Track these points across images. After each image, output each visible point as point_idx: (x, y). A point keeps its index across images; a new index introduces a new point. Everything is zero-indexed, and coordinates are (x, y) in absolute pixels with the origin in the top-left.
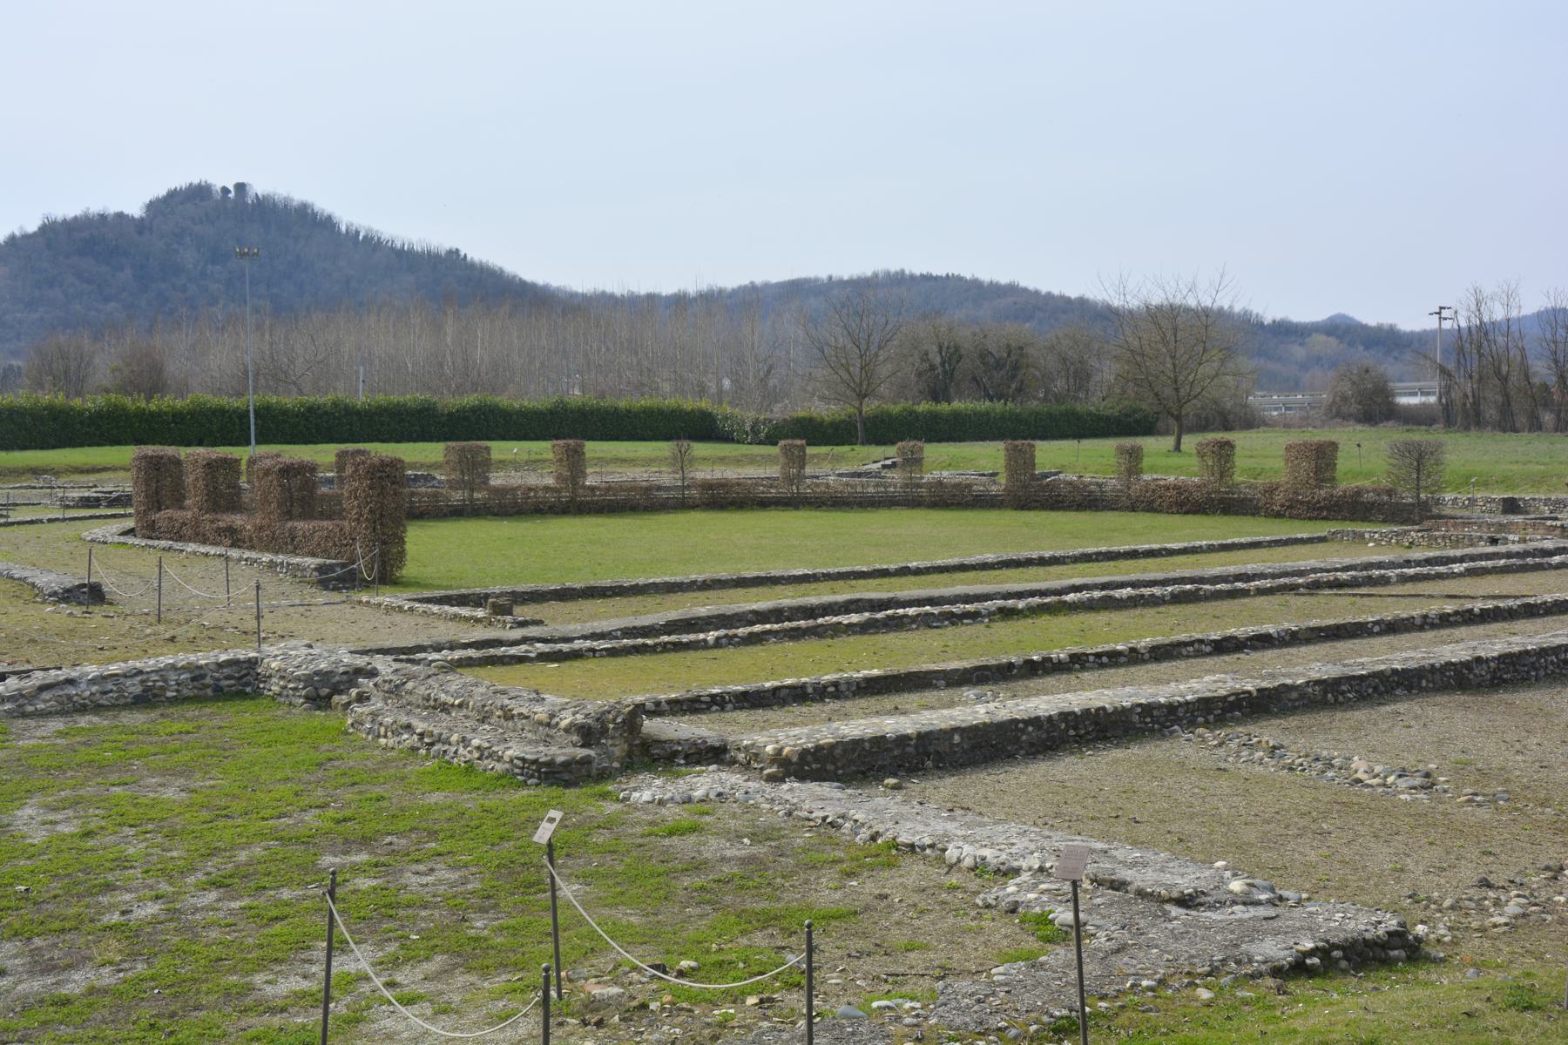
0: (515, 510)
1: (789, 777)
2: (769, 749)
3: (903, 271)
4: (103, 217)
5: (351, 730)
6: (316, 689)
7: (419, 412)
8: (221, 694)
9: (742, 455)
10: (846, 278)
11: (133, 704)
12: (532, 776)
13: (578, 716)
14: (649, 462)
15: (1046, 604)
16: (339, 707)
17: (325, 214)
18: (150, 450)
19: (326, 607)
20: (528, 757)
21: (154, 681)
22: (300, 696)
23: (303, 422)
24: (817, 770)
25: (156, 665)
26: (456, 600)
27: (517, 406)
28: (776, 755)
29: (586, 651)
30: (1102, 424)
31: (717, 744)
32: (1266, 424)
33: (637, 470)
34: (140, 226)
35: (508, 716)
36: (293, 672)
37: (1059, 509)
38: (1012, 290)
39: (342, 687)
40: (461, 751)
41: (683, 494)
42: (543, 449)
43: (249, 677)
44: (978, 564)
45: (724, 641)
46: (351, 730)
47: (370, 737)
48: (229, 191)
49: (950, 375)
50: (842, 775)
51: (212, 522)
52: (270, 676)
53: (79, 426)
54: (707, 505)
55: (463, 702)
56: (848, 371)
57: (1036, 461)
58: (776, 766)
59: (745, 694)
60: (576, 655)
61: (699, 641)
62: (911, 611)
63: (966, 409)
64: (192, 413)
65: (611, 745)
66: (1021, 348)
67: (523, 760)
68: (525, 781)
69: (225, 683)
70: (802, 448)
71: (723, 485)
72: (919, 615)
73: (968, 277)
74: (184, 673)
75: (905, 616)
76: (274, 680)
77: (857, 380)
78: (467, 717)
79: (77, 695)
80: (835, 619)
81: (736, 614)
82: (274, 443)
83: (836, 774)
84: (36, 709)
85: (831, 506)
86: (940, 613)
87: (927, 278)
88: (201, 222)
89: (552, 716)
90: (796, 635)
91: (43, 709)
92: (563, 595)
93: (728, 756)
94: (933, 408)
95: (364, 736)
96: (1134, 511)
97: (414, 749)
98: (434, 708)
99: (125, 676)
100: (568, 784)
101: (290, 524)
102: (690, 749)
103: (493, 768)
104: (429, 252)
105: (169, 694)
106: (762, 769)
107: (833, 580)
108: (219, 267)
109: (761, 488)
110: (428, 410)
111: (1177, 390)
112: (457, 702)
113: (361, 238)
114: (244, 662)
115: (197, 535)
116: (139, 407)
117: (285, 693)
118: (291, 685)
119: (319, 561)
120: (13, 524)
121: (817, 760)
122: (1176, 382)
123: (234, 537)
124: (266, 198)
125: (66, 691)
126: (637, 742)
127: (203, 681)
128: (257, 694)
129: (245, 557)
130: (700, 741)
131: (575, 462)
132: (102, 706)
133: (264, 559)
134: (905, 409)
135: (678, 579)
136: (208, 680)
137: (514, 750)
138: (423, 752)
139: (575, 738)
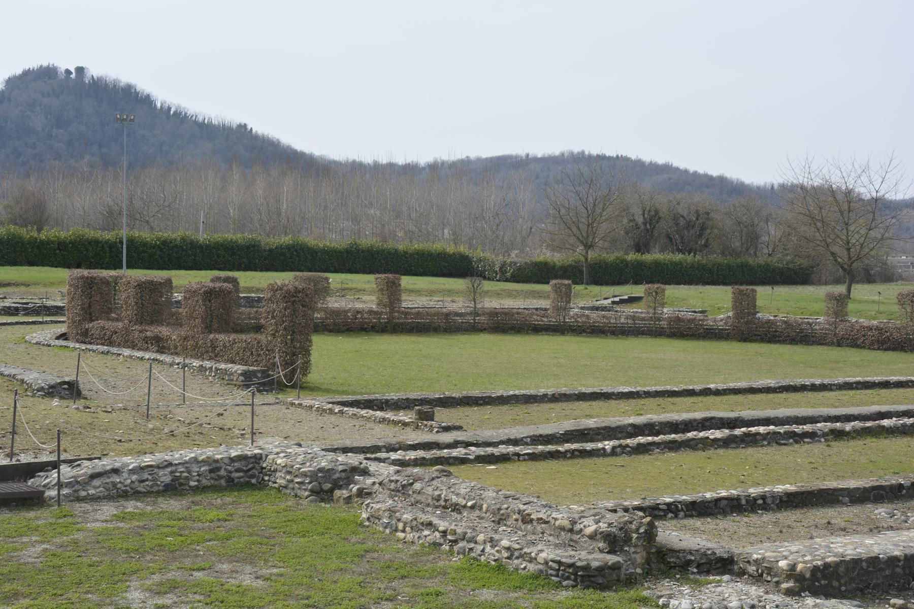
0: (345, 328)
1: (804, 592)
2: (783, 564)
3: (583, 152)
5: (367, 523)
6: (320, 483)
7: (248, 247)
8: (232, 485)
10: (539, 156)
11: (163, 491)
12: (568, 578)
13: (601, 524)
14: (431, 293)
15: (868, 428)
16: (341, 500)
17: (145, 93)
18: (85, 272)
19: (264, 407)
20: (564, 560)
21: (181, 472)
22: (305, 490)
23: (158, 252)
24: (826, 586)
25: (181, 459)
27: (321, 246)
28: (791, 570)
29: (513, 455)
30: (769, 275)
31: (726, 556)
32: (903, 279)
33: (424, 299)
35: (526, 519)
36: (300, 469)
37: (775, 342)
38: (667, 169)
39: (341, 483)
40: (488, 549)
41: (474, 320)
43: (254, 471)
44: (763, 388)
45: (618, 450)
46: (367, 523)
47: (388, 531)
48: (71, 73)
49: (650, 232)
50: (845, 591)
51: (140, 332)
52: (275, 471)
54: (493, 329)
56: (579, 229)
57: (757, 304)
58: (792, 581)
60: (504, 458)
61: (599, 450)
62: (762, 429)
63: (664, 259)
64: (73, 243)
65: (633, 553)
66: (708, 214)
67: (559, 563)
69: (235, 475)
70: (569, 287)
71: (508, 313)
72: (768, 433)
73: (633, 157)
74: (204, 466)
75: (758, 434)
76: (278, 474)
77: (585, 235)
78: (481, 518)
79: (120, 482)
80: (702, 434)
81: (618, 427)
82: (136, 268)
83: (840, 590)
84: (88, 494)
85: (590, 333)
86: (785, 433)
87: (601, 158)
88: (49, 95)
89: (574, 523)
90: (673, 446)
91: (94, 495)
92: (446, 403)
93: (736, 567)
94: (638, 258)
95: (381, 529)
96: (839, 346)
97: (436, 545)
98: (445, 507)
99: (158, 467)
100: (603, 588)
101: (211, 336)
102: (701, 558)
103: (525, 568)
105: (192, 483)
106: (777, 583)
107: (652, 397)
108: (61, 131)
109: (535, 317)
110: (254, 246)
111: (849, 250)
112: (469, 504)
113: (172, 112)
114: (251, 457)
115: (127, 342)
116: (31, 236)
117: (291, 486)
118: (299, 480)
119: (245, 368)
121: (825, 577)
122: (848, 243)
123: (160, 344)
124: (100, 79)
125: (111, 480)
126: (653, 550)
127: (219, 473)
128: (262, 486)
129: (177, 362)
130: (709, 552)
131: (392, 292)
132: (139, 492)
133: (194, 364)
134: (617, 258)
135: (532, 392)
136: (222, 473)
137: (548, 554)
138: (446, 547)
139: (601, 545)
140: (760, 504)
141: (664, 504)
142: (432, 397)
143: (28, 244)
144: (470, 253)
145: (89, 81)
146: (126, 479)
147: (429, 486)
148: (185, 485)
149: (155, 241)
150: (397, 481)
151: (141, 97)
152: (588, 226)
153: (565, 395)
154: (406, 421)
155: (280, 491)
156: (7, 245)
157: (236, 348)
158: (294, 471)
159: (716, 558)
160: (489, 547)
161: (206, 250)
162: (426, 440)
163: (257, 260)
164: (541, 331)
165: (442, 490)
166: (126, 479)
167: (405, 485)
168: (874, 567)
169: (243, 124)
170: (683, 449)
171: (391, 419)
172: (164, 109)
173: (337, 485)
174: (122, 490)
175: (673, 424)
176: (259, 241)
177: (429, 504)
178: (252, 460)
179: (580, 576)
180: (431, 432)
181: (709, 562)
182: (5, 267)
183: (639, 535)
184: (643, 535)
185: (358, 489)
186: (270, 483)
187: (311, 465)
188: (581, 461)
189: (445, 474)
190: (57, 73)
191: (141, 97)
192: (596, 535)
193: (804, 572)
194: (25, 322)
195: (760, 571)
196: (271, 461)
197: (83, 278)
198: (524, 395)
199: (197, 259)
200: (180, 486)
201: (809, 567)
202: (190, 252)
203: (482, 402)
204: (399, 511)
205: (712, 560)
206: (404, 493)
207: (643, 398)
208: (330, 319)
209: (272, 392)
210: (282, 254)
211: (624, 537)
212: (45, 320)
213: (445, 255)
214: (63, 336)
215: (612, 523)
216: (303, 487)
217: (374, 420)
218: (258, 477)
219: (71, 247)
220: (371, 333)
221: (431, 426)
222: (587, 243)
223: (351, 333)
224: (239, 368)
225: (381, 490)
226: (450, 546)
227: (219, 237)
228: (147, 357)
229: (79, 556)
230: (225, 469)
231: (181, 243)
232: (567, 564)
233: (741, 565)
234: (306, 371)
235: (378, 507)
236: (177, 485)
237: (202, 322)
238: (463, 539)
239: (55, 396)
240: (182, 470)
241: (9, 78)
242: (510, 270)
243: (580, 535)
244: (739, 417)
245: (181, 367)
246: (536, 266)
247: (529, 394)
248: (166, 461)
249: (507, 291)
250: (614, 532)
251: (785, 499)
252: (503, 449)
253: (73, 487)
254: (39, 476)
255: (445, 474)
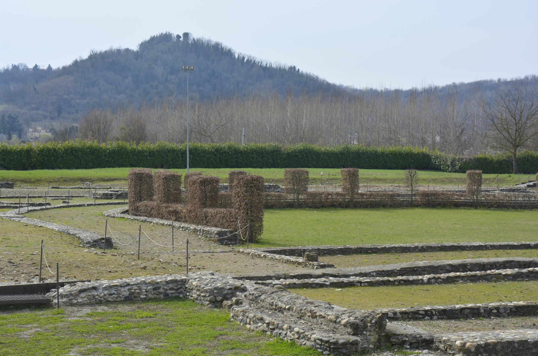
2: (458, 343)
4: (119, 51)
5: (232, 320)
6: (215, 297)
7: (273, 152)
8: (167, 298)
9: (445, 178)
10: (508, 80)
11: (124, 301)
12: (326, 350)
13: (351, 318)
14: (393, 181)
16: (227, 307)
17: (228, 49)
18: (137, 170)
20: (324, 339)
21: (135, 290)
22: (207, 300)
23: (213, 157)
26: (288, 252)
27: (323, 149)
28: (462, 346)
31: (428, 338)
34: (136, 55)
35: (314, 316)
39: (228, 297)
40: (289, 333)
41: (412, 199)
42: (336, 173)
43: (181, 289)
45: (433, 280)
46: (232, 320)
47: (242, 324)
52: (192, 289)
53: (104, 157)
54: (425, 205)
55: (290, 307)
56: (508, 132)
59: (444, 311)
60: (351, 285)
61: (418, 280)
64: (158, 151)
65: (369, 335)
67: (321, 340)
68: (322, 352)
69: (169, 292)
70: (480, 175)
71: (435, 194)
74: (149, 286)
76: (194, 291)
77: (513, 137)
78: (292, 315)
79: (97, 295)
81: (440, 266)
82: (199, 167)
84: (78, 301)
85: (496, 207)
89: (337, 317)
90: (474, 279)
91: (81, 302)
92: (345, 252)
93: (434, 345)
97: (264, 331)
98: (275, 310)
99: (121, 286)
101: (205, 210)
102: (413, 340)
103: (305, 344)
104: (280, 68)
105: (142, 297)
107: (496, 249)
109: (456, 197)
110: (276, 151)
112: (287, 307)
113: (245, 61)
114: (179, 281)
118: (203, 294)
119: (219, 229)
120: (71, 206)
123: (177, 216)
124: (198, 40)
125: (92, 293)
126: (383, 334)
127: (159, 291)
128: (185, 298)
130: (418, 336)
131: (353, 180)
133: (191, 228)
135: (408, 245)
136: (161, 290)
139: (349, 330)
140: (495, 313)
141: (423, 311)
142: (336, 248)
143: (130, 153)
144: (431, 153)
145: (192, 42)
146: (101, 293)
147: (269, 297)
148: (138, 297)
149: (211, 149)
150: (253, 294)
151: (225, 51)
152: (516, 131)
153: (431, 247)
154: (300, 262)
155: (194, 301)
156: (118, 154)
157: (218, 217)
158: (200, 289)
159: (422, 340)
160: (289, 332)
161: (245, 154)
162: (303, 273)
163: (279, 161)
164: (460, 206)
165: (275, 299)
166: (101, 293)
167: (257, 296)
168: (523, 347)
169: (293, 67)
170: (480, 281)
171: (292, 261)
172: (240, 59)
173: (225, 298)
174: (98, 300)
175: (481, 265)
176: (280, 148)
177: (267, 308)
178: (180, 283)
179: (332, 348)
180: (313, 268)
181: (418, 342)
182: (115, 168)
183: (372, 324)
184: (374, 324)
185: (236, 300)
186: (190, 297)
187: (211, 285)
188: (403, 287)
189: (281, 290)
190: (171, 38)
191: (225, 51)
192: (347, 324)
193: (470, 348)
194: (113, 203)
195: (446, 347)
196: (190, 284)
197: (135, 174)
198: (401, 247)
199: (239, 160)
200: (135, 298)
201: (474, 345)
202: (234, 156)
203: (371, 251)
204: (248, 312)
205: (419, 341)
206: (256, 301)
207: (490, 250)
208: (310, 199)
209: (236, 245)
210: (296, 156)
211: (363, 325)
212: (125, 202)
213: (411, 154)
214: (126, 212)
215: (357, 317)
216: (206, 299)
217: (282, 261)
218: (184, 293)
219: (157, 155)
220: (338, 208)
221: (313, 265)
222: (515, 144)
223: (325, 208)
224: (215, 230)
225: (245, 300)
226: (271, 332)
227: (253, 145)
228: (166, 223)
229: (54, 335)
230: (163, 288)
231: (228, 150)
232: (325, 341)
233: (437, 344)
234: (260, 231)
235: (237, 310)
236: (133, 298)
237: (199, 201)
238: (277, 328)
239: (97, 247)
240: (136, 288)
241: (142, 43)
242: (458, 164)
243: (339, 325)
244: (532, 261)
245: (184, 230)
246: (477, 161)
247: (405, 246)
248: (126, 283)
249: (450, 179)
250: (357, 323)
251: (514, 310)
252: (352, 279)
253: (68, 297)
254: (52, 291)
255: (281, 290)
